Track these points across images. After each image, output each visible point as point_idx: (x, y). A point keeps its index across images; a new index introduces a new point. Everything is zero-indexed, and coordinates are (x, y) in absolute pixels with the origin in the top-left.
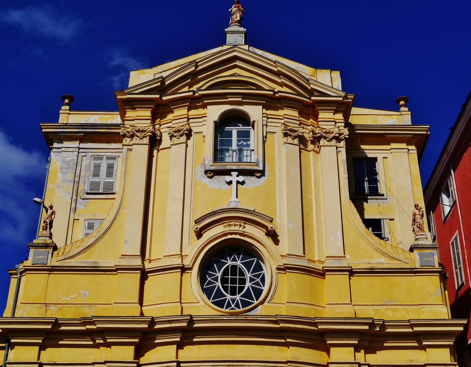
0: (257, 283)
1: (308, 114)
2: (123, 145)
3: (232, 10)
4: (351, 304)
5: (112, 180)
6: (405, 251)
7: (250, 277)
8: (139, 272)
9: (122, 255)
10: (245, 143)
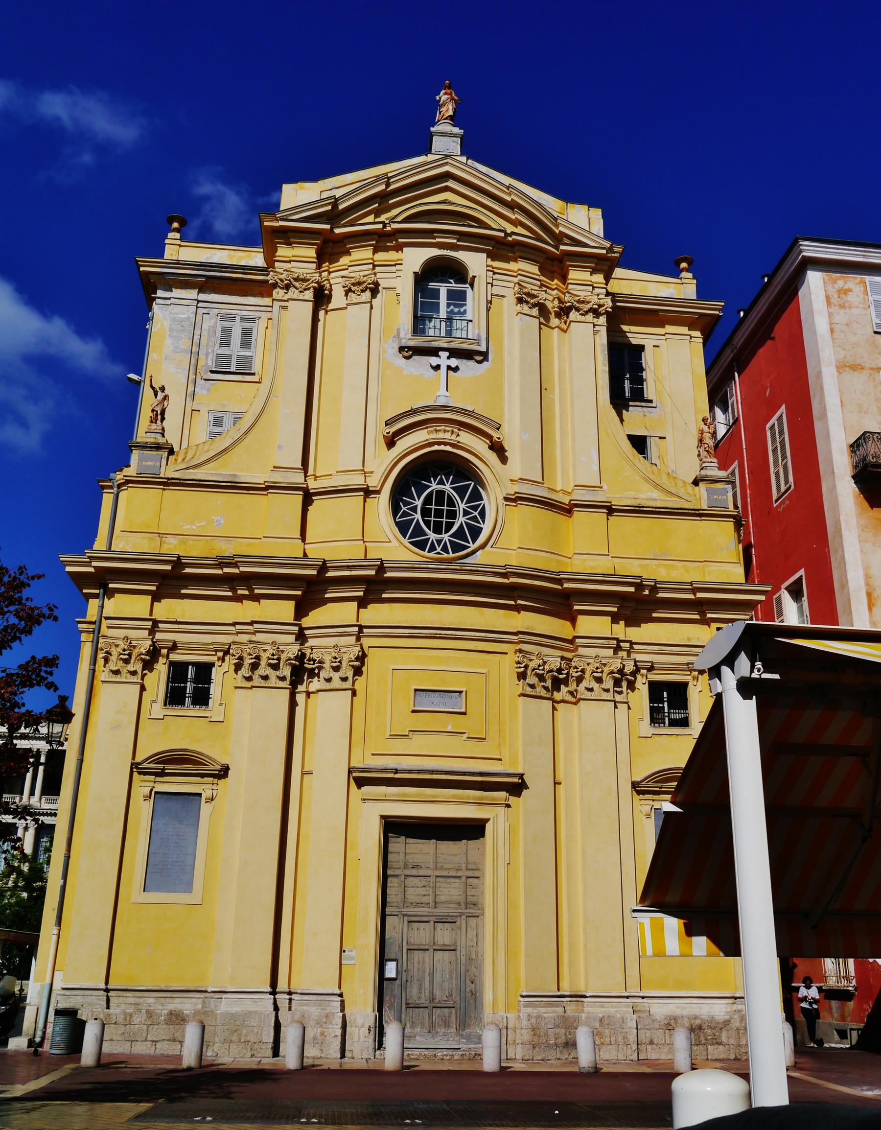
0: (474, 519)
1: (552, 272)
2: (273, 300)
3: (440, 98)
4: (608, 555)
5: (250, 354)
8: (301, 493)
9: (275, 467)
10: (456, 310)
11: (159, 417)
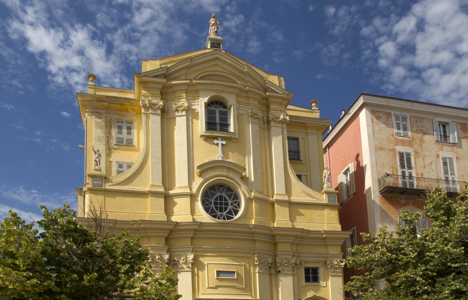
0: (235, 207)
6: (4, 219)
7: (231, 203)
11: (98, 163)
